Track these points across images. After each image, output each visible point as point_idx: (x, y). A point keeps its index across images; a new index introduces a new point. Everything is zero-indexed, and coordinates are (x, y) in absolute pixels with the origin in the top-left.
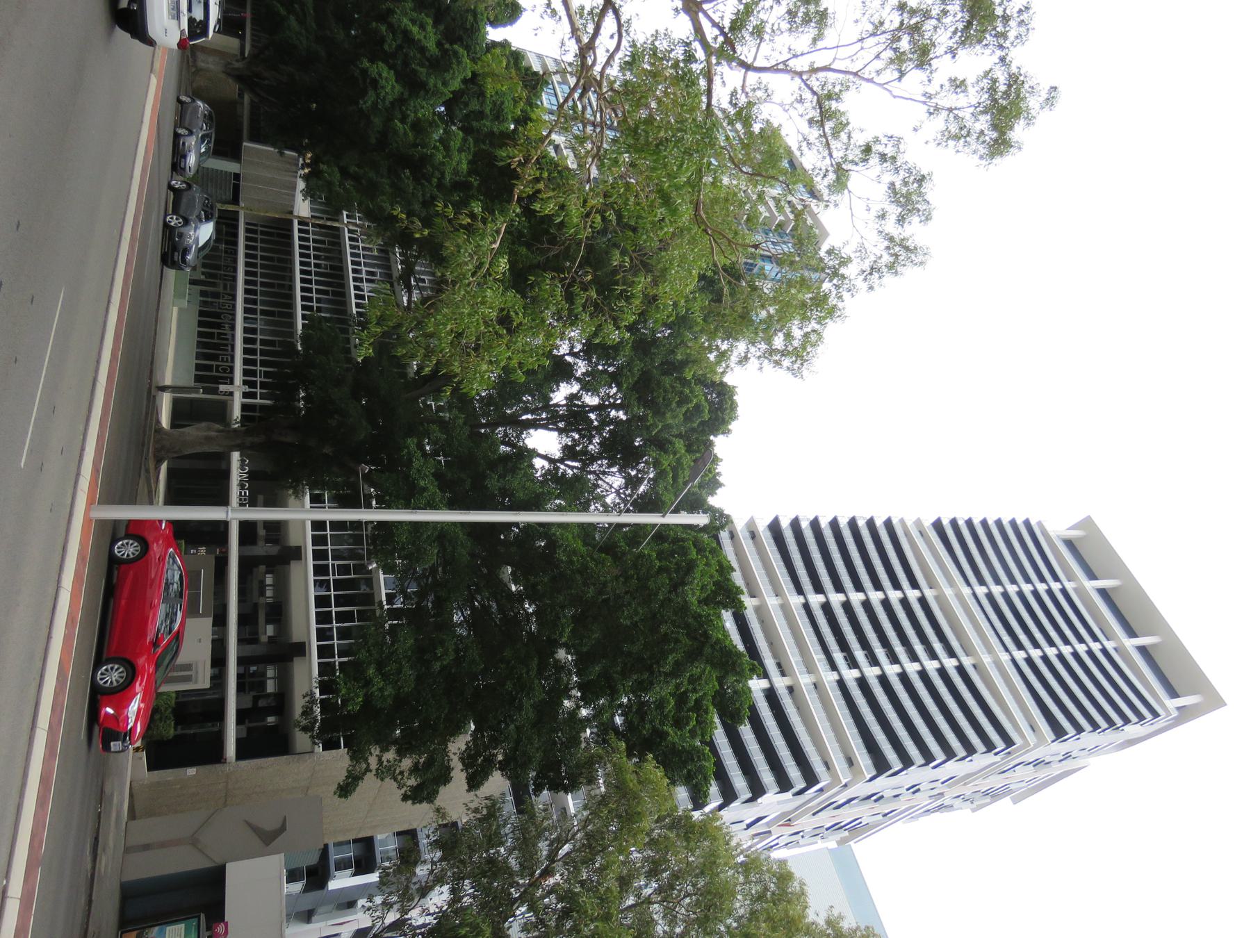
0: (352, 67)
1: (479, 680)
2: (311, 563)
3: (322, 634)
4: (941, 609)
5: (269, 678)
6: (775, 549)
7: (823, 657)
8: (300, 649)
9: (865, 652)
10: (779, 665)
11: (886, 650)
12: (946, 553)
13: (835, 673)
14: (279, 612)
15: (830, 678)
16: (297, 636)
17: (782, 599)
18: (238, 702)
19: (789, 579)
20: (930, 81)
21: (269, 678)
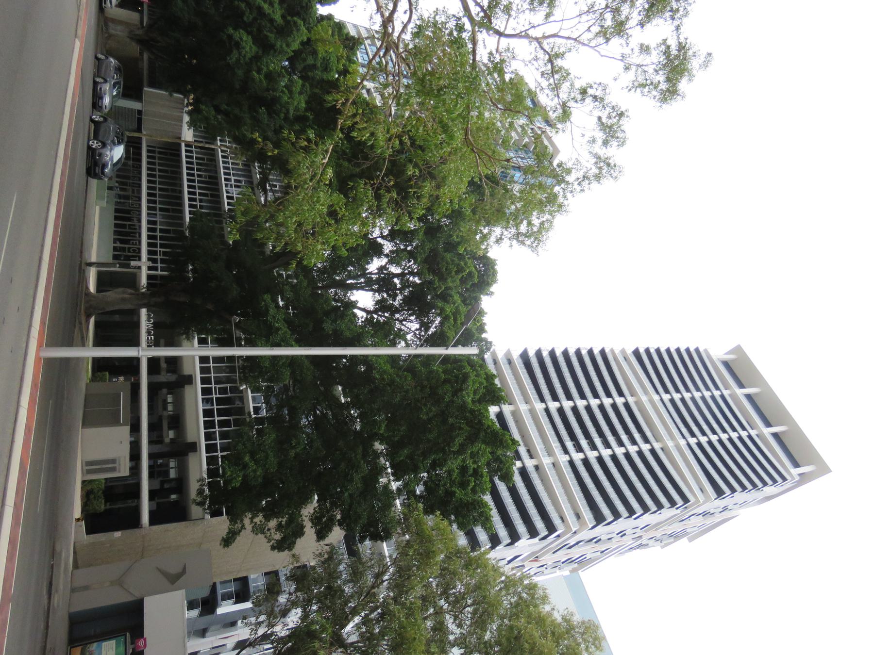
3: (208, 436)
8: (193, 447)
10: (529, 451)
13: (567, 456)
14: (177, 421)
16: (190, 438)
17: (531, 406)
21: (173, 468)
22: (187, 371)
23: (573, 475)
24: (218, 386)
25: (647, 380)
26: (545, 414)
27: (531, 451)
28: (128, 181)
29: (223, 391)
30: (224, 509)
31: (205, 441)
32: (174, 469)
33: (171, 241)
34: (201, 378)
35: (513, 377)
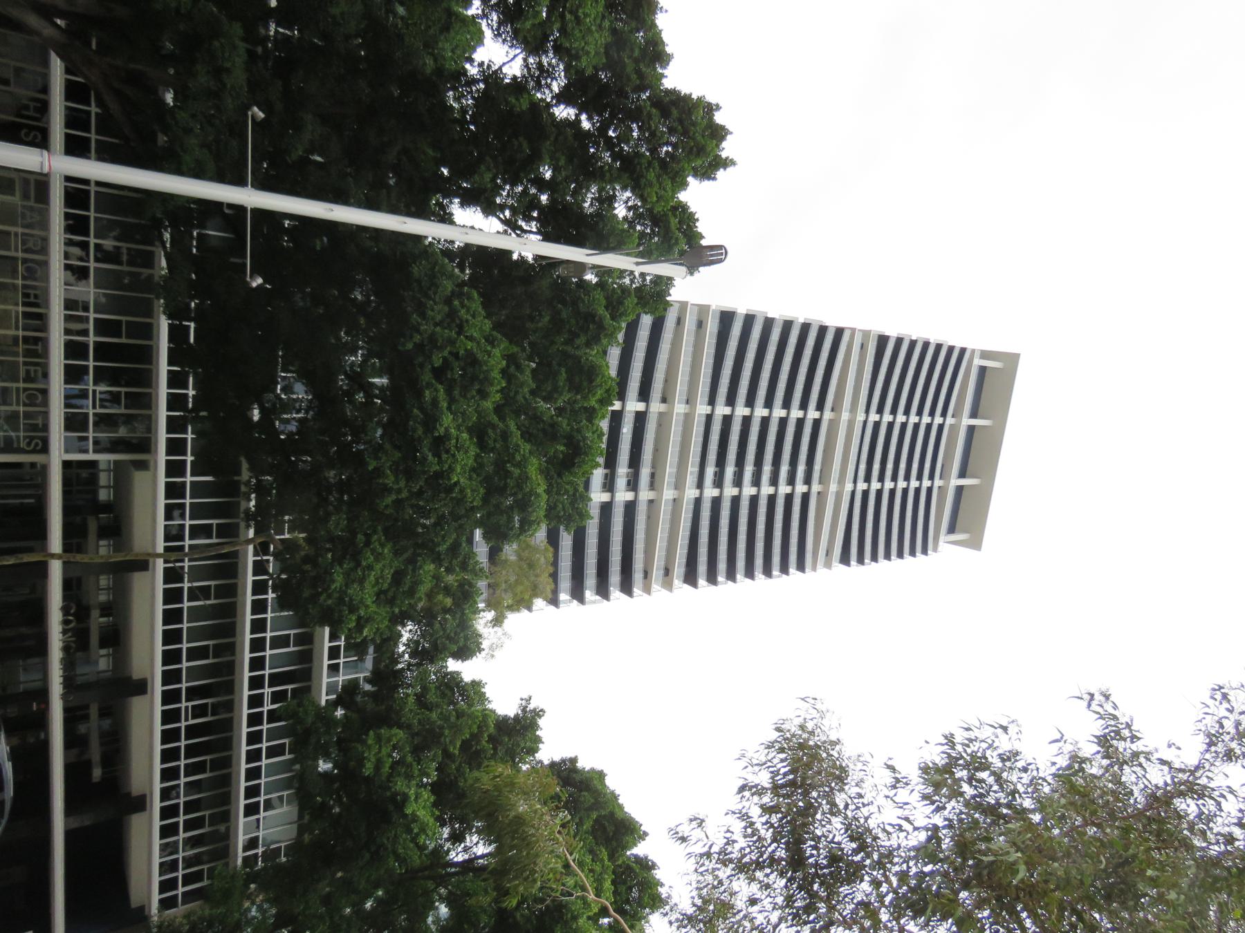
0: (327, 630)
1: (331, 798)
2: (162, 480)
3: (169, 677)
4: (824, 451)
5: (103, 487)
6: (714, 341)
7: (696, 469)
8: (141, 687)
9: (737, 469)
10: (653, 475)
11: (755, 468)
12: (870, 377)
13: (698, 492)
14: (116, 638)
15: (703, 409)
16: (137, 673)
17: (691, 408)
18: (66, 757)
19: (708, 389)
20: (1179, 748)
21: (103, 487)
22: (136, 787)
23: (689, 524)
24: (190, 704)
25: (867, 392)
26: (704, 419)
27: (656, 477)
28: (15, 385)
29: (198, 711)
30: (191, 379)
31: (168, 432)
32: (104, 548)
33: (116, 362)
34: (169, 441)
35: (689, 369)
